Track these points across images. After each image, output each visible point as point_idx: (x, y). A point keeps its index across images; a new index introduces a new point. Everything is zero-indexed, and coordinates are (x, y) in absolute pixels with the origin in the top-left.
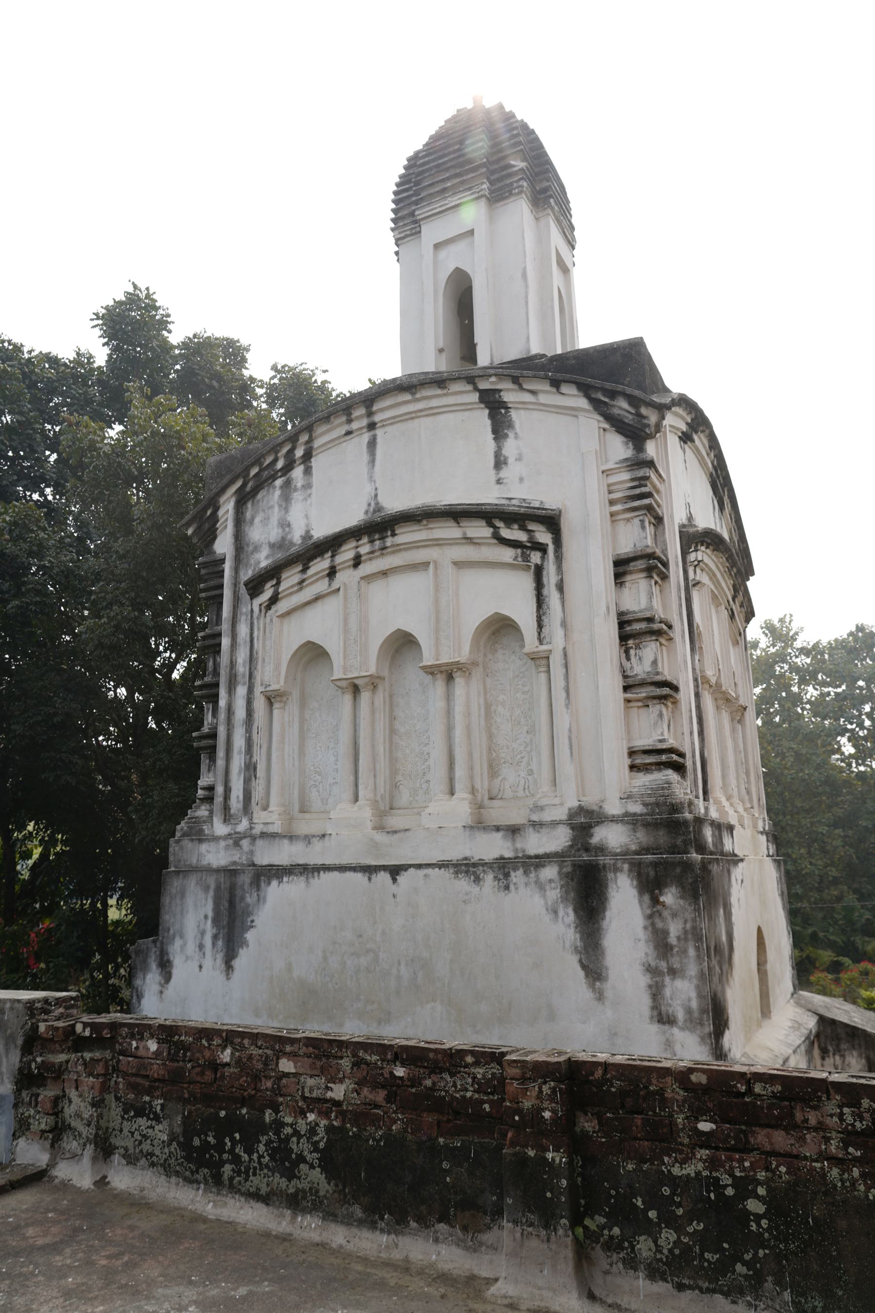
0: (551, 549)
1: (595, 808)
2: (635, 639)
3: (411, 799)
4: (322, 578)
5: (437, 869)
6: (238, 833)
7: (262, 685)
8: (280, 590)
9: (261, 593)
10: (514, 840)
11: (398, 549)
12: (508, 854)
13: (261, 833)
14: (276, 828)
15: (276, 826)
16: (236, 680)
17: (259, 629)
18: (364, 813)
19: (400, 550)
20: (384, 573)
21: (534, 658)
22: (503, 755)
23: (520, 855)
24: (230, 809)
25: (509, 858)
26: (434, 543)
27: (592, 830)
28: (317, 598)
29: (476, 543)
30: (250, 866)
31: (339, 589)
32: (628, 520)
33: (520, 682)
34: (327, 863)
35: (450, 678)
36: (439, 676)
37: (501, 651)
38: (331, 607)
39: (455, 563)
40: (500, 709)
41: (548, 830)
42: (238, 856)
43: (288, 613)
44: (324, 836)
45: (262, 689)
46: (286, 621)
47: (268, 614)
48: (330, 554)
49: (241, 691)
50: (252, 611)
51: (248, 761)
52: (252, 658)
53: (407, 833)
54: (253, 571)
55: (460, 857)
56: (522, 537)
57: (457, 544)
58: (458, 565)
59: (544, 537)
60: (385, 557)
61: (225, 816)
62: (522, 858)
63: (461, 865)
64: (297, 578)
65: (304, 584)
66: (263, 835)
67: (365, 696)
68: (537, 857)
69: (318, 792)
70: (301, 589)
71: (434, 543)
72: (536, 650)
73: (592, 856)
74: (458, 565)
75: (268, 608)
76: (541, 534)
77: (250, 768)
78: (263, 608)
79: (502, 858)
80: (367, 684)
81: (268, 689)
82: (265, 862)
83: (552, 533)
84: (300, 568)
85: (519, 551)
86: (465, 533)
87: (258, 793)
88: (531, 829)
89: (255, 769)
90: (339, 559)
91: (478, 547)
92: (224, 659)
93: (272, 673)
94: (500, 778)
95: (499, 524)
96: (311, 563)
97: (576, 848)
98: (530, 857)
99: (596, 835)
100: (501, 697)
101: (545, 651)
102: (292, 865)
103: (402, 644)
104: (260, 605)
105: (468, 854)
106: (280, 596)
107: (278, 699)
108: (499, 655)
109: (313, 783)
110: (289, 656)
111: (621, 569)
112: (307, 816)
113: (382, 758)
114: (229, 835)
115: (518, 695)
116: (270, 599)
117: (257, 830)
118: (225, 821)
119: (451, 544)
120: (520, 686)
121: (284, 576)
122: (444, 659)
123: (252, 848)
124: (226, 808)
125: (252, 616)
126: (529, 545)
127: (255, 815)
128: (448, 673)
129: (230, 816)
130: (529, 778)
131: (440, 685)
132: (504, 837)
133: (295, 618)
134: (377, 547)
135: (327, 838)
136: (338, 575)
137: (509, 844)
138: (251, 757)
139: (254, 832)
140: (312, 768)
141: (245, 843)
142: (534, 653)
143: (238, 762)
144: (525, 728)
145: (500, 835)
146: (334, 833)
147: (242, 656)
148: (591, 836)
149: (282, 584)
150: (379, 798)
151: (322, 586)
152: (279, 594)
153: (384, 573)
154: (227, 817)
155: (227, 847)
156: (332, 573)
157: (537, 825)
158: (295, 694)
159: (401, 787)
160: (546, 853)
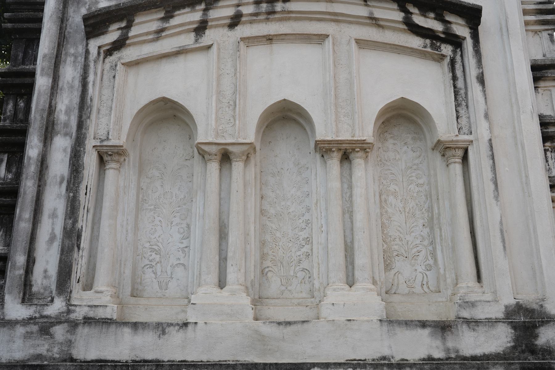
0: (469, 44)
1: (535, 306)
3: (283, 288)
4: (188, 31)
8: (131, 34)
9: (103, 33)
10: (444, 339)
11: (288, 16)
12: (438, 354)
13: (85, 318)
14: (111, 311)
15: (108, 310)
16: (53, 128)
17: (95, 74)
18: (237, 298)
19: (289, 19)
20: (270, 39)
21: (444, 149)
22: (396, 247)
23: (453, 356)
24: (31, 286)
25: (439, 359)
26: (333, 17)
27: (537, 331)
29: (380, 26)
30: (65, 361)
31: (209, 47)
33: (414, 174)
34: (189, 358)
35: (346, 157)
37: (391, 141)
38: (196, 64)
39: (358, 41)
40: (391, 199)
41: (485, 329)
42: (46, 347)
43: (137, 63)
46: (132, 72)
47: (107, 60)
48: (203, 6)
49: (61, 144)
50: (87, 52)
53: (305, 325)
55: (377, 355)
56: (438, 27)
58: (361, 43)
59: (461, 29)
61: (24, 294)
62: (455, 359)
64: (155, 26)
65: (164, 34)
66: (88, 321)
67: (238, 167)
69: (155, 273)
70: (157, 39)
71: (333, 17)
72: (455, 139)
73: (539, 359)
74: (361, 43)
76: (458, 26)
77: (72, 237)
79: (430, 359)
80: (243, 153)
81: (105, 143)
82: (92, 355)
83: (470, 28)
84: (162, 15)
85: (428, 41)
86: (371, 13)
87: (80, 267)
88: (465, 327)
89: (79, 237)
90: (213, 14)
91: (381, 30)
94: (393, 272)
96: (177, 12)
97: (519, 349)
98: (465, 358)
99: (541, 335)
100: (392, 187)
101: (464, 141)
102: (134, 361)
103: (286, 117)
104: (100, 47)
105: (386, 352)
106: (128, 42)
107: (116, 158)
108: (390, 143)
109: (147, 262)
111: (538, 74)
112: (142, 301)
114: (31, 319)
116: (114, 43)
117: (79, 314)
118: (23, 301)
119: (351, 23)
120: (414, 178)
121: (138, 20)
122: (345, 136)
123: (69, 336)
125: (86, 58)
127: (74, 295)
128: (346, 152)
130: (428, 273)
131: (334, 162)
132: (432, 335)
133: (144, 71)
134: (263, 10)
135: (190, 327)
136: (207, 32)
137: (438, 342)
138: (75, 221)
139: (72, 316)
140: (147, 245)
141: (59, 331)
142: (452, 141)
143: (51, 226)
144: (421, 222)
145: (426, 332)
146: (201, 323)
147: (66, 102)
148: (536, 337)
150: (249, 285)
151: (188, 40)
152: (128, 38)
153: (270, 39)
154: (27, 295)
155: (28, 336)
156: (201, 28)
157: (473, 323)
158: (133, 156)
159: (270, 274)
160: (484, 355)
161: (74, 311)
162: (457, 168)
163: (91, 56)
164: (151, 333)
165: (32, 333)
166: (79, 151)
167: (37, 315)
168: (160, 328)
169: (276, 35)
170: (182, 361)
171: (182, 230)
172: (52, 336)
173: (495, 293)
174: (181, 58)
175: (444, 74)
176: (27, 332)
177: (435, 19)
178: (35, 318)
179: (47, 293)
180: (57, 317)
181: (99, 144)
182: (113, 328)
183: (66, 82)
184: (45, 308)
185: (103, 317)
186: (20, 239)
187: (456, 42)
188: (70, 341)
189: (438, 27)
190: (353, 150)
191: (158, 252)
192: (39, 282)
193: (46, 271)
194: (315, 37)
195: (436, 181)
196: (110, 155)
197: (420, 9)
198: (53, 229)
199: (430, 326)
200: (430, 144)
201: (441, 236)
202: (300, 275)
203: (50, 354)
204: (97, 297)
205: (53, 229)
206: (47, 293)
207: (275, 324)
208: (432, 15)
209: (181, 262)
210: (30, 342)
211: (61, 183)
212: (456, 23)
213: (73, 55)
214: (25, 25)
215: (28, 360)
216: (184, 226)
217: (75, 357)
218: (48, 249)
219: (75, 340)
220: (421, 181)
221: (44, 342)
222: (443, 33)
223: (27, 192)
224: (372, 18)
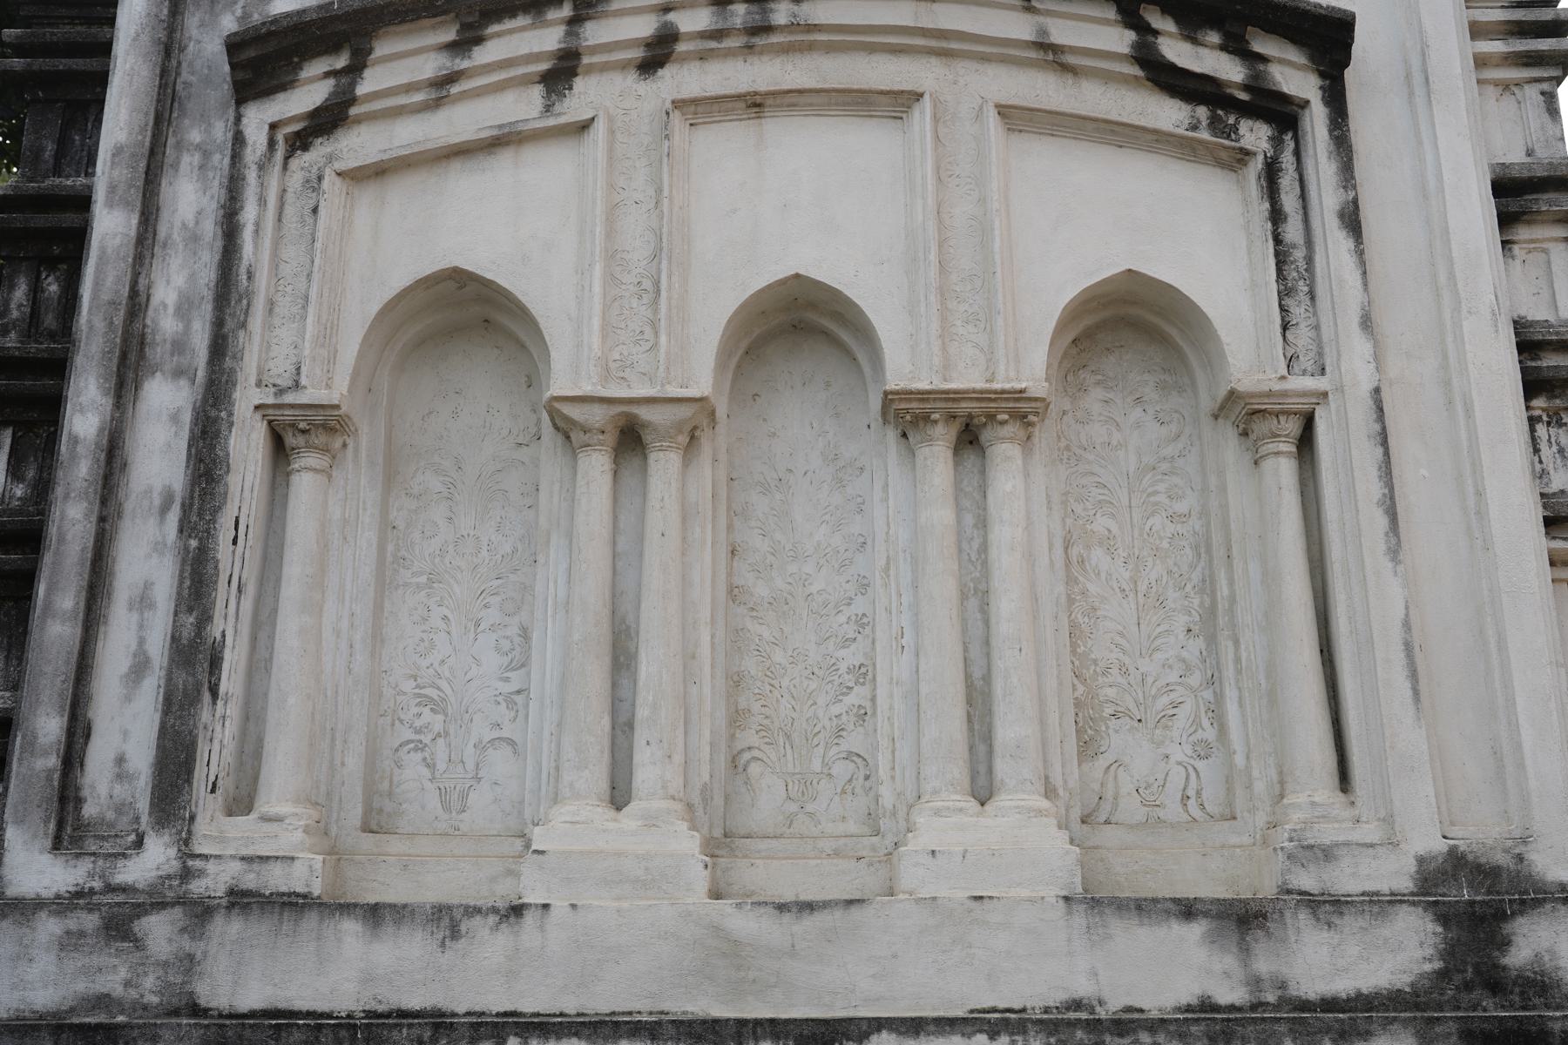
0: (1317, 119)
1: (1502, 859)
2: (1552, 397)
3: (793, 807)
4: (525, 81)
5: (982, 1039)
6: (124, 889)
7: (259, 384)
8: (362, 89)
9: (283, 87)
10: (1245, 951)
12: (1230, 993)
14: (305, 873)
17: (262, 202)
18: (662, 837)
19: (811, 47)
20: (755, 104)
21: (1246, 415)
23: (1271, 998)
24: (79, 801)
25: (1232, 1008)
26: (933, 43)
27: (1507, 928)
28: (502, 141)
29: (1066, 68)
30: (176, 1012)
31: (584, 127)
32: (1506, 86)
33: (1161, 487)
35: (969, 439)
36: (940, 430)
37: (1098, 393)
38: (547, 174)
39: (1004, 111)
40: (1097, 555)
42: (123, 973)
43: (379, 172)
44: (517, 910)
45: (259, 396)
46: (367, 196)
47: (295, 163)
48: (566, 11)
49: (165, 401)
50: (239, 140)
51: (187, 633)
52: (227, 289)
53: (855, 911)
54: (245, 16)
55: (1056, 997)
56: (1230, 70)
57: (1004, 60)
58: (1014, 117)
59: (1294, 77)
60: (755, 60)
62: (1277, 1007)
63: (1073, 1024)
64: (430, 66)
65: (455, 89)
66: (241, 900)
67: (664, 464)
68: (1330, 1004)
69: (431, 766)
71: (933, 43)
72: (1277, 387)
73: (1512, 1007)
74: (1014, 117)
75: (300, 142)
76: (1288, 71)
77: (194, 662)
78: (280, 137)
79: (1207, 1006)
80: (679, 427)
81: (289, 398)
82: (252, 996)
83: (1322, 75)
84: (449, 35)
85: (1202, 112)
86: (1043, 32)
87: (217, 751)
88: (1304, 916)
89: (215, 663)
90: (596, 33)
92: (101, 277)
93: (308, 341)
94: (1102, 762)
95: (1158, 21)
96: (494, 28)
97: (1458, 979)
98: (1304, 1005)
99: (1518, 940)
100: (1101, 524)
101: (1304, 394)
102: (371, 1014)
103: (800, 324)
104: (273, 127)
105: (1082, 988)
106: (353, 111)
107: (320, 439)
108: (1094, 399)
110: (375, 308)
111: (1513, 206)
112: (395, 845)
113: (707, 669)
114: (79, 894)
115: (1156, 521)
116: (315, 114)
117: (214, 881)
118: (57, 845)
119: (985, 58)
120: (1162, 498)
121: (381, 48)
122: (967, 379)
123: (187, 944)
124: (67, 795)
125: (236, 157)
126: (1243, 96)
127: (202, 827)
129: (82, 827)
130: (1201, 765)
131: (937, 453)
132: (1212, 939)
133: (401, 193)
134: (738, 22)
135: (529, 918)
136: (579, 83)
137: (1230, 961)
138: (205, 619)
139: (197, 887)
140: (409, 686)
141: (159, 930)
142: (1270, 394)
144: (1181, 621)
145: (1195, 930)
147: (178, 282)
148: (1505, 944)
149: (367, 73)
150: (696, 799)
151: (524, 106)
152: (353, 101)
153: (755, 104)
154: (68, 827)
155: (70, 942)
156: (561, 72)
157: (1326, 906)
158: (367, 436)
159: (754, 769)
160: (1359, 995)
161: (201, 873)
162: (1283, 470)
163: (249, 150)
164: (419, 935)
165: (82, 934)
166: (216, 420)
167: (97, 884)
168: (446, 921)
169: (774, 94)
170: (506, 1014)
171: (506, 645)
172: (138, 943)
173: (1388, 820)
174: (505, 158)
175: (1246, 202)
176: (68, 933)
177: (1223, 48)
178: (92, 892)
179: (124, 823)
180: (152, 890)
181: (271, 400)
182: (311, 920)
183: (177, 224)
184: (120, 863)
185: (284, 889)
186: (49, 669)
187: (1282, 114)
188: (191, 957)
189: (1230, 70)
190: (991, 417)
191: (438, 707)
192: (103, 790)
193: (120, 760)
194: (883, 99)
195: (1224, 507)
196: (303, 432)
197: (1179, 21)
198: (141, 641)
199: (1206, 914)
200: (1207, 403)
201: (1238, 660)
202: (842, 770)
203: (133, 994)
204: (266, 833)
205: (141, 641)
206: (124, 823)
207: (770, 910)
208: (1214, 38)
209: (505, 734)
210: (77, 961)
211: (164, 509)
212: (1282, 61)
213: (198, 147)
214: (63, 64)
215: (72, 1010)
216: (513, 631)
217: (203, 1002)
218: (128, 699)
219: (205, 954)
220: (1181, 507)
221: (115, 961)
222: (1246, 87)
223: (69, 537)
224: (1044, 46)
